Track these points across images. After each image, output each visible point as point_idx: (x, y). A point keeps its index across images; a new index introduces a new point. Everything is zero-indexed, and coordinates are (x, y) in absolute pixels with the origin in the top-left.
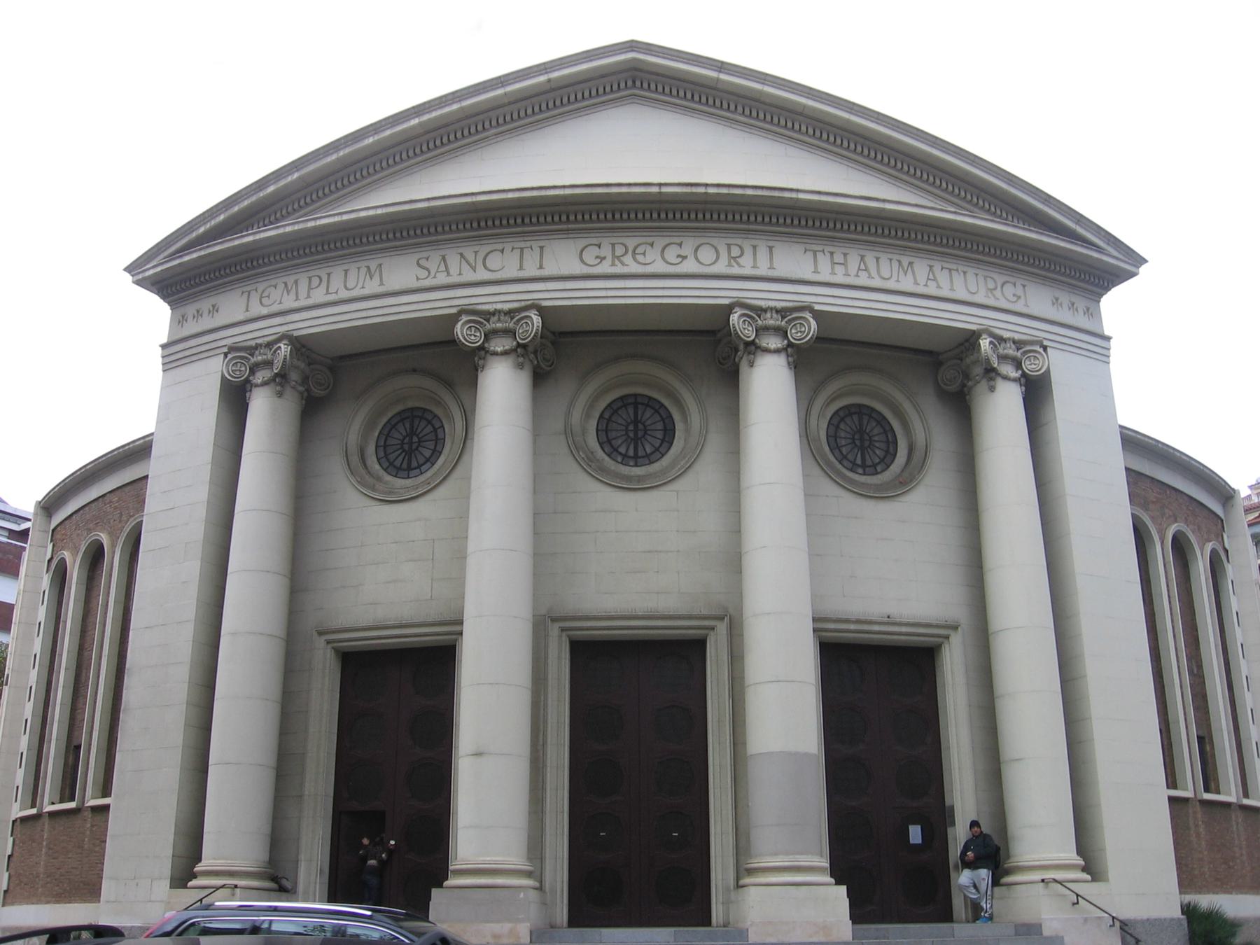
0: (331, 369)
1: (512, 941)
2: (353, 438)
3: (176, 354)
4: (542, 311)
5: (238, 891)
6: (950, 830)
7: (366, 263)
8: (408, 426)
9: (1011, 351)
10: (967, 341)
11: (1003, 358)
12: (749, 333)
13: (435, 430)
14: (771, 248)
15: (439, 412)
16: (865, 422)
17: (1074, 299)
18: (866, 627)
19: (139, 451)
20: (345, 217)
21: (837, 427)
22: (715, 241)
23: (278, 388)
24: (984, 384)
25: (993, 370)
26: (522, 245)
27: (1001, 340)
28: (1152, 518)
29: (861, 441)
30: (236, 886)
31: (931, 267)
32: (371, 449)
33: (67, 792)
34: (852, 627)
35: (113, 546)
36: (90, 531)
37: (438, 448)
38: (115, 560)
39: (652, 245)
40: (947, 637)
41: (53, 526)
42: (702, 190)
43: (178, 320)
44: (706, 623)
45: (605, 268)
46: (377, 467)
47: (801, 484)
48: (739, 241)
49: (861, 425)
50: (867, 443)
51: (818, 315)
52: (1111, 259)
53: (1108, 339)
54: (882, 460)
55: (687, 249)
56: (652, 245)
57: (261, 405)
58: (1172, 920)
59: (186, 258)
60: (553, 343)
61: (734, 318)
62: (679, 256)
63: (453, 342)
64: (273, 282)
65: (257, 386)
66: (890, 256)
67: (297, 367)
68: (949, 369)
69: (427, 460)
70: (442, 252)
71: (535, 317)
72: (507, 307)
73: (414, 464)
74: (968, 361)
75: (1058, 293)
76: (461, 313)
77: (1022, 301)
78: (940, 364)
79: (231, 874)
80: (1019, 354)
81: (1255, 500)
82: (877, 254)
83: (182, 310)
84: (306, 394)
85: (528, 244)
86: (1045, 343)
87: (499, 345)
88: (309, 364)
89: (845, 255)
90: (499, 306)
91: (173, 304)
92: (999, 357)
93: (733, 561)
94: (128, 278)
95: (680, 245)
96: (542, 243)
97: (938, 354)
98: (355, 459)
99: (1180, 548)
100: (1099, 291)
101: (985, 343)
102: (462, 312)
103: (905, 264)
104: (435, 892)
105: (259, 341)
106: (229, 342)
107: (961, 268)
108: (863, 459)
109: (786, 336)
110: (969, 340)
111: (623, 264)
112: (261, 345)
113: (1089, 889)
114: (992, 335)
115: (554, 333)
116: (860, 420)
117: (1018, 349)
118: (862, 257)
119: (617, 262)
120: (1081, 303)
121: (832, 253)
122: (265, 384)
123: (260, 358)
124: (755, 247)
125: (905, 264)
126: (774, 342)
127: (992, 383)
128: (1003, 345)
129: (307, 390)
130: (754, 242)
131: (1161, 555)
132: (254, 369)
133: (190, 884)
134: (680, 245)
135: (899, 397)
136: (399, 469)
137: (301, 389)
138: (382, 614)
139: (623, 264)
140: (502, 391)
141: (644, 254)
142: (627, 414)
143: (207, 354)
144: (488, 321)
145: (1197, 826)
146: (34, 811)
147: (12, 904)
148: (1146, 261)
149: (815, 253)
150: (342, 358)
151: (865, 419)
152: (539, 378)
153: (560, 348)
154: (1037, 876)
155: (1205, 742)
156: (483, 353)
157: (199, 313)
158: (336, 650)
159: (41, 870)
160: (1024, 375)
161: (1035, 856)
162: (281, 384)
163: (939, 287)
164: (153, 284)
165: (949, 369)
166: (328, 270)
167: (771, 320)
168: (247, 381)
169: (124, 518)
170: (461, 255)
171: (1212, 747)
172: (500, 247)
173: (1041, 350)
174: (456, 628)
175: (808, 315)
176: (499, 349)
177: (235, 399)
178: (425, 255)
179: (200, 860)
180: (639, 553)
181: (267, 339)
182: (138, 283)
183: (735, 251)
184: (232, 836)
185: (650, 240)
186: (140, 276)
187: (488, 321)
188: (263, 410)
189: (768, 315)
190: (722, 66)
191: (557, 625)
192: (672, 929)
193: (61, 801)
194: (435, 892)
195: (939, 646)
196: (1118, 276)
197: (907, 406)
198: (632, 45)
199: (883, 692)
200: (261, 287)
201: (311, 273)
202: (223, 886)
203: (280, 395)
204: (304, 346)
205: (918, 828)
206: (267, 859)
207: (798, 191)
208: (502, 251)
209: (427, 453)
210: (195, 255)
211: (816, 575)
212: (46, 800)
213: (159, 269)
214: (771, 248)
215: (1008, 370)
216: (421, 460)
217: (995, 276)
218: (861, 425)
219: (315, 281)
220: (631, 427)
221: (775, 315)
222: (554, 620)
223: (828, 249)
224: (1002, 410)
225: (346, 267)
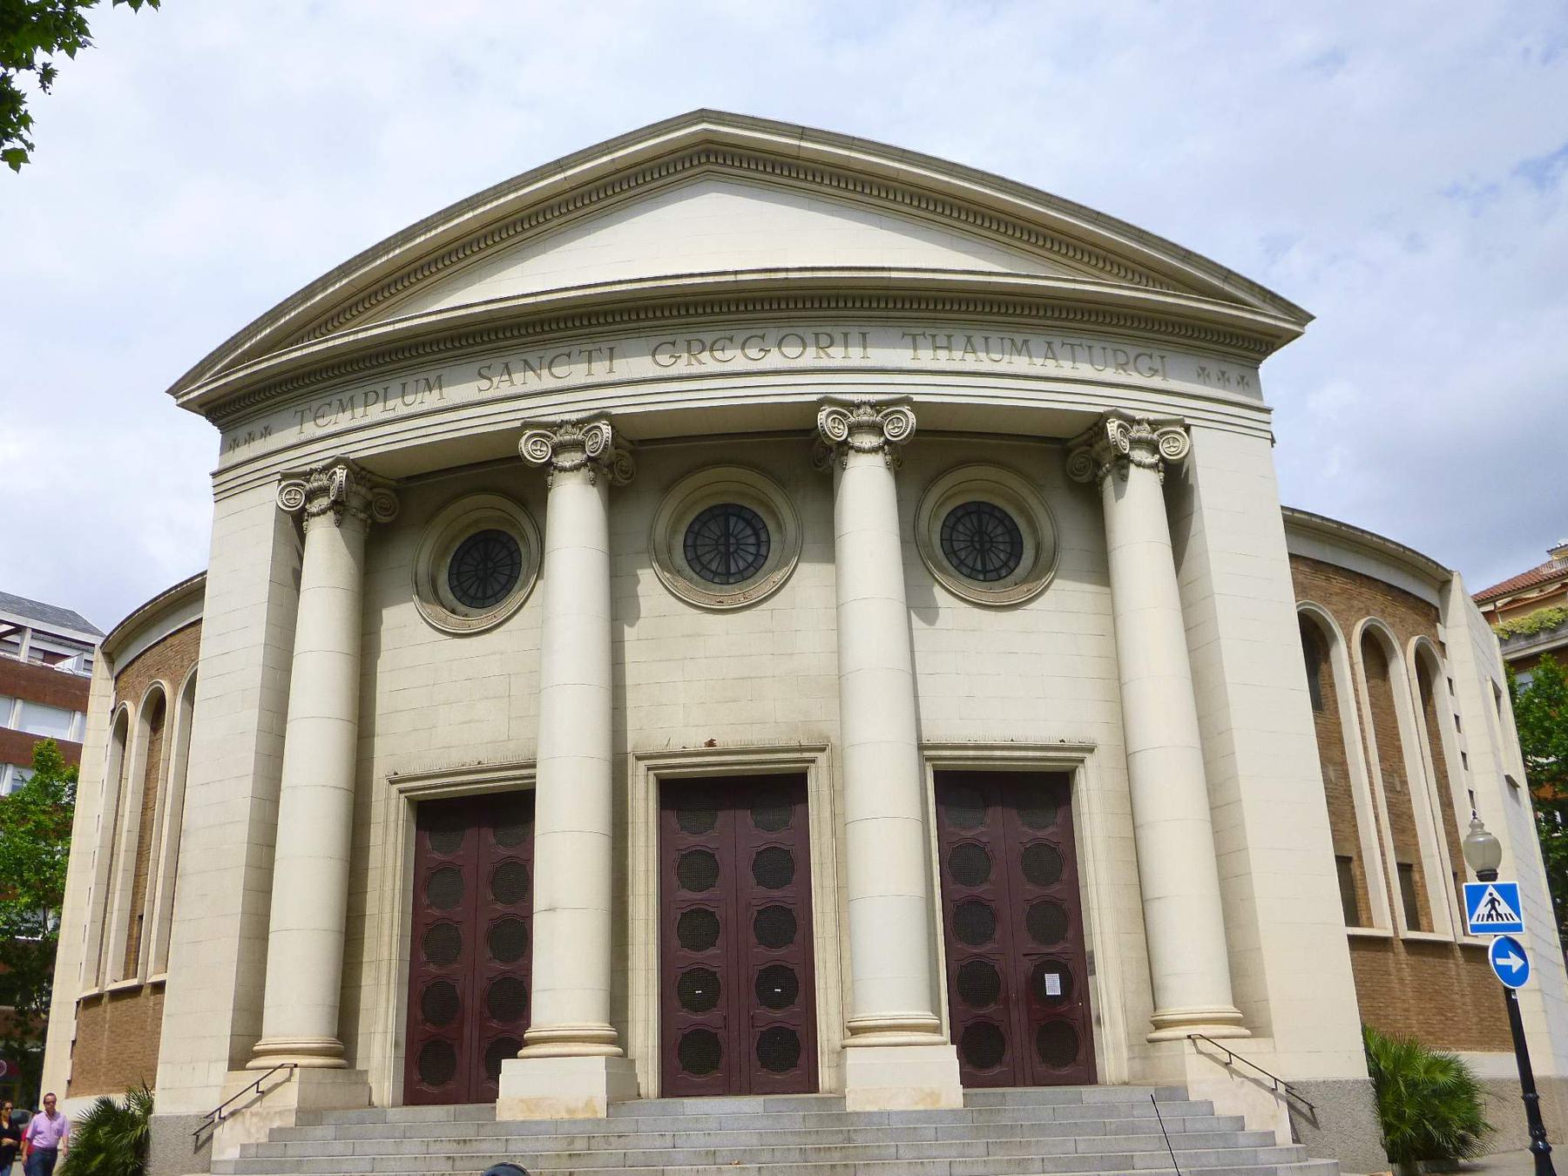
0: (396, 491)
1: (588, 1115)
2: (423, 568)
3: (226, 483)
4: (613, 420)
5: (297, 1070)
7: (425, 375)
9: (1144, 432)
10: (1096, 424)
11: (1137, 443)
12: (841, 432)
14: (864, 335)
17: (1224, 367)
18: (392, 818)
19: (190, 593)
20: (397, 326)
22: (800, 331)
25: (1127, 457)
26: (590, 347)
27: (1133, 421)
28: (1335, 612)
31: (1049, 344)
32: (443, 578)
33: (132, 967)
34: (971, 753)
35: (175, 694)
36: (152, 677)
38: (175, 707)
40: (1082, 761)
42: (731, 278)
44: (806, 755)
46: (451, 596)
47: (903, 599)
48: (828, 330)
49: (980, 526)
50: (987, 546)
51: (917, 407)
52: (1268, 318)
53: (1268, 411)
54: (1005, 564)
58: (1356, 1082)
60: (631, 452)
61: (821, 416)
63: (519, 458)
64: (327, 400)
65: (314, 515)
66: (1002, 335)
67: (357, 493)
68: (1078, 461)
70: (505, 360)
71: (604, 427)
72: (574, 417)
73: (490, 592)
74: (1097, 447)
75: (1204, 363)
78: (1070, 451)
80: (1155, 436)
81: (1559, 568)
82: (986, 334)
83: (232, 434)
86: (1188, 421)
87: (566, 460)
89: (949, 337)
90: (566, 417)
91: (224, 429)
92: (1131, 442)
93: (838, 686)
95: (763, 337)
96: (612, 344)
97: (1067, 440)
98: (426, 588)
99: (1376, 651)
100: (1257, 356)
101: (1112, 427)
102: (527, 425)
103: (1019, 344)
104: (506, 1064)
105: (313, 466)
107: (1085, 342)
108: (984, 564)
109: (882, 434)
110: (1097, 424)
111: (700, 362)
113: (1247, 1048)
114: (1120, 416)
115: (632, 442)
116: (980, 521)
117: (1154, 431)
118: (969, 338)
120: (1234, 372)
121: (934, 336)
122: (323, 512)
124: (846, 335)
125: (1019, 344)
126: (868, 441)
128: (1136, 427)
129: (370, 517)
130: (845, 330)
131: (1346, 658)
133: (249, 1065)
134: (763, 337)
135: (1025, 491)
137: (362, 516)
139: (700, 362)
140: (574, 513)
142: (715, 529)
143: (262, 481)
146: (95, 991)
147: (76, 1095)
148: (1312, 318)
149: (914, 336)
150: (410, 478)
151: (985, 518)
153: (636, 463)
154: (1182, 1032)
155: (1407, 870)
159: (103, 1056)
160: (1163, 459)
161: (1182, 1009)
164: (201, 406)
165: (1078, 461)
166: (385, 385)
167: (865, 416)
168: (303, 509)
169: (186, 663)
170: (526, 362)
171: (1422, 878)
173: (1181, 430)
176: (567, 464)
177: (295, 524)
178: (487, 363)
179: (259, 1037)
181: (321, 464)
182: (182, 405)
183: (824, 340)
184: (296, 1010)
185: (728, 334)
188: (323, 536)
190: (803, 132)
191: (642, 764)
192: (761, 1098)
193: (126, 977)
194: (506, 1064)
196: (1278, 342)
197: (1033, 502)
198: (702, 115)
199: (1007, 827)
201: (367, 389)
202: (281, 1066)
204: (363, 469)
207: (890, 269)
209: (503, 579)
212: (108, 977)
213: (204, 390)
214: (864, 335)
216: (497, 587)
217: (1128, 349)
218: (980, 526)
219: (372, 396)
220: (722, 540)
221: (869, 410)
223: (929, 331)
224: (1137, 505)
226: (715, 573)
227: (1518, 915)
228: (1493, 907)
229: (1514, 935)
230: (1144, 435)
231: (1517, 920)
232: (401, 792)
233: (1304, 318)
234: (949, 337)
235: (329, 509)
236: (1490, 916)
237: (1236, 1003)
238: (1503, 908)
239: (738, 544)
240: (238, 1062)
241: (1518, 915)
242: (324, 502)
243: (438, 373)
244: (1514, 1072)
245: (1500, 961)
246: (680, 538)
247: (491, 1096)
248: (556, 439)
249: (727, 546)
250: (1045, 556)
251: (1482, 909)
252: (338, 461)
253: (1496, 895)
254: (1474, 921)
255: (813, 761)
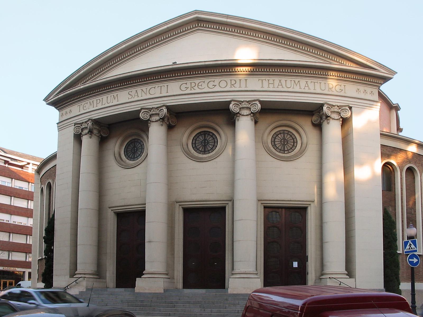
3: (61, 125)
6: (307, 263)
8: (133, 145)
9: (336, 109)
13: (141, 145)
15: (142, 140)
16: (286, 136)
21: (275, 138)
23: (90, 136)
24: (326, 121)
26: (161, 85)
29: (284, 142)
30: (85, 277)
32: (122, 152)
36: (48, 179)
37: (142, 151)
39: (204, 82)
41: (41, 177)
43: (61, 115)
45: (188, 91)
46: (125, 157)
50: (286, 143)
52: (382, 73)
55: (217, 82)
56: (204, 82)
57: (85, 140)
59: (60, 96)
61: (231, 105)
62: (213, 85)
63: (139, 118)
64: (86, 102)
65: (84, 135)
67: (95, 128)
69: (139, 155)
72: (156, 106)
73: (135, 157)
74: (321, 113)
76: (142, 109)
77: (343, 91)
79: (85, 274)
83: (62, 112)
84: (100, 137)
85: (163, 85)
86: (351, 106)
87: (154, 118)
88: (100, 128)
89: (274, 80)
94: (45, 103)
95: (214, 81)
104: (137, 279)
106: (74, 122)
112: (154, 108)
114: (328, 104)
118: (280, 80)
119: (192, 89)
122: (86, 134)
123: (84, 126)
126: (245, 112)
127: (328, 121)
132: (82, 130)
133: (74, 277)
136: (131, 158)
138: (194, 198)
141: (201, 85)
144: (150, 111)
145: (403, 262)
146: (41, 258)
147: (39, 282)
148: (397, 73)
151: (286, 135)
152: (170, 128)
156: (149, 121)
157: (66, 113)
158: (115, 212)
162: (90, 134)
163: (309, 89)
166: (102, 97)
167: (244, 105)
168: (81, 134)
172: (154, 86)
174: (144, 206)
175: (257, 103)
177: (78, 138)
178: (131, 90)
179: (77, 270)
180: (202, 181)
182: (48, 104)
186: (47, 102)
187: (82, 126)
189: (244, 103)
190: (228, 16)
195: (307, 207)
198: (196, 12)
200: (83, 103)
201: (97, 99)
202: (81, 277)
203: (91, 137)
204: (97, 122)
205: (297, 263)
206: (96, 270)
208: (155, 88)
210: (62, 95)
211: (258, 186)
215: (335, 116)
221: (246, 103)
222: (177, 202)
224: (333, 130)
225: (107, 96)
226: (201, 151)
227: (416, 248)
228: (410, 246)
229: (415, 253)
230: (336, 110)
231: (416, 249)
232: (112, 210)
233: (394, 73)
234: (274, 80)
235: (88, 133)
236: (409, 249)
237: (346, 269)
238: (413, 246)
239: (281, 142)
240: (72, 275)
241: (416, 248)
242: (86, 131)
243: (117, 94)
244: (410, 288)
245: (410, 260)
246: (190, 141)
247: (133, 286)
248: (151, 113)
249: (205, 142)
250: (304, 146)
251: (408, 247)
252: (89, 119)
253: (411, 243)
254: (405, 251)
255: (227, 204)
